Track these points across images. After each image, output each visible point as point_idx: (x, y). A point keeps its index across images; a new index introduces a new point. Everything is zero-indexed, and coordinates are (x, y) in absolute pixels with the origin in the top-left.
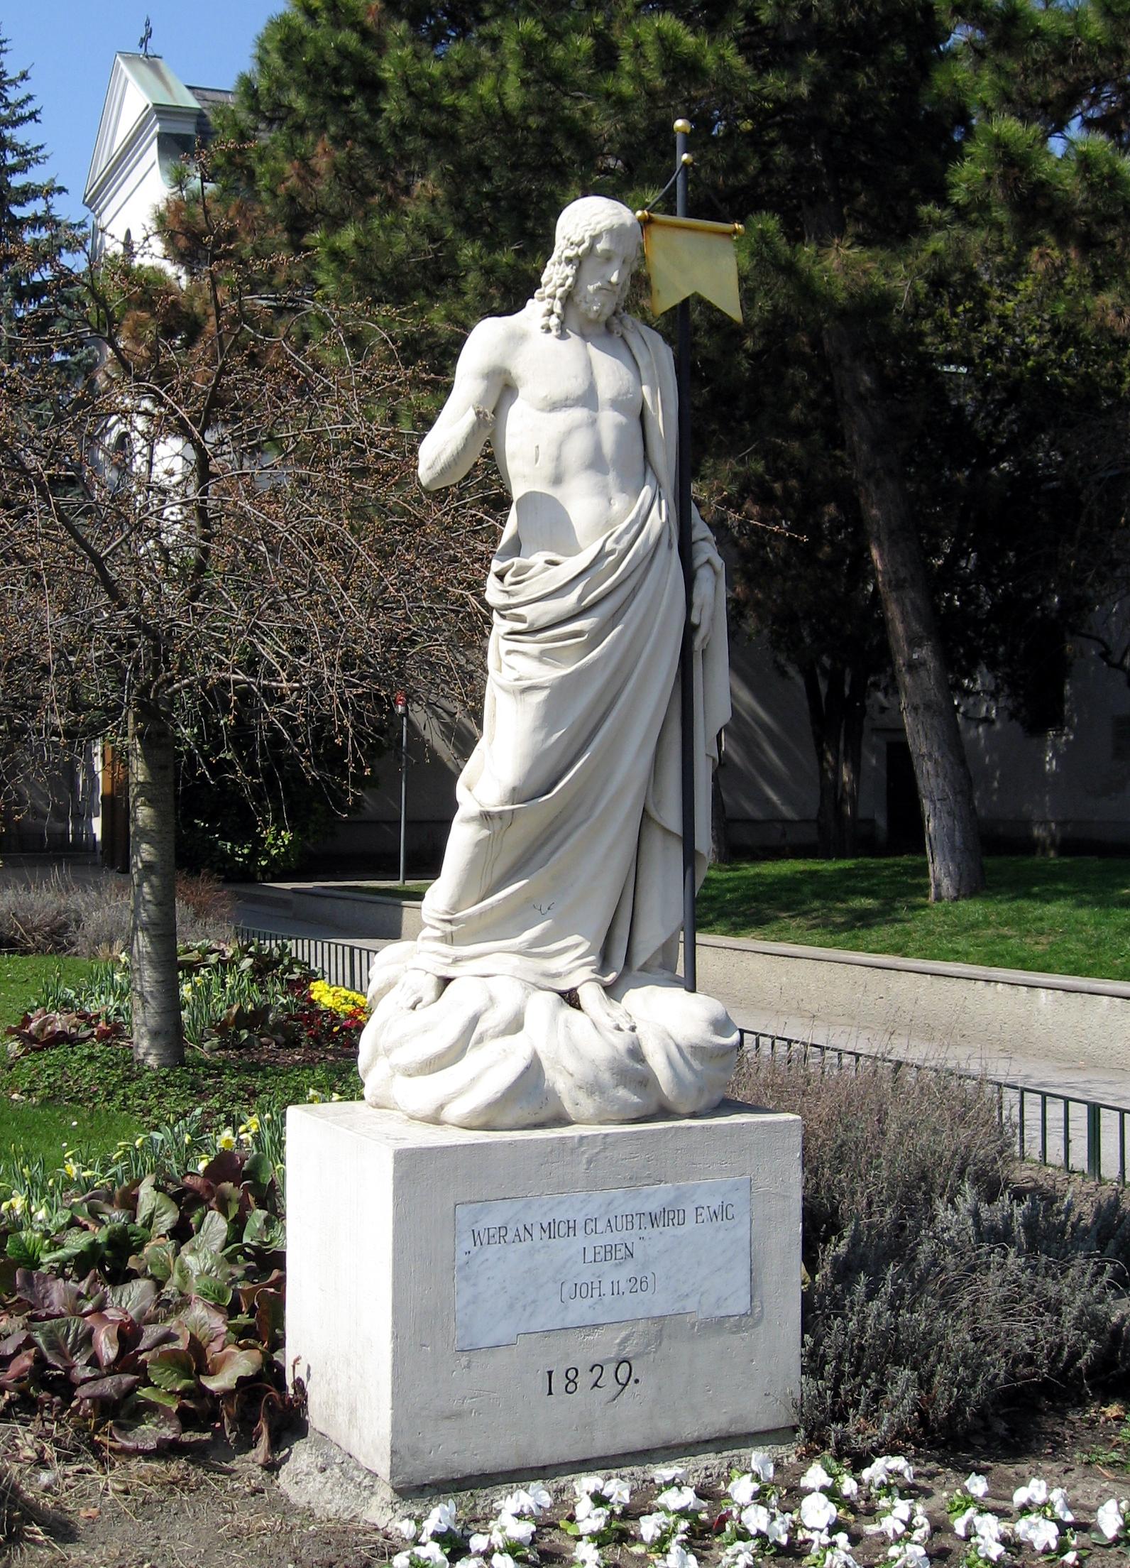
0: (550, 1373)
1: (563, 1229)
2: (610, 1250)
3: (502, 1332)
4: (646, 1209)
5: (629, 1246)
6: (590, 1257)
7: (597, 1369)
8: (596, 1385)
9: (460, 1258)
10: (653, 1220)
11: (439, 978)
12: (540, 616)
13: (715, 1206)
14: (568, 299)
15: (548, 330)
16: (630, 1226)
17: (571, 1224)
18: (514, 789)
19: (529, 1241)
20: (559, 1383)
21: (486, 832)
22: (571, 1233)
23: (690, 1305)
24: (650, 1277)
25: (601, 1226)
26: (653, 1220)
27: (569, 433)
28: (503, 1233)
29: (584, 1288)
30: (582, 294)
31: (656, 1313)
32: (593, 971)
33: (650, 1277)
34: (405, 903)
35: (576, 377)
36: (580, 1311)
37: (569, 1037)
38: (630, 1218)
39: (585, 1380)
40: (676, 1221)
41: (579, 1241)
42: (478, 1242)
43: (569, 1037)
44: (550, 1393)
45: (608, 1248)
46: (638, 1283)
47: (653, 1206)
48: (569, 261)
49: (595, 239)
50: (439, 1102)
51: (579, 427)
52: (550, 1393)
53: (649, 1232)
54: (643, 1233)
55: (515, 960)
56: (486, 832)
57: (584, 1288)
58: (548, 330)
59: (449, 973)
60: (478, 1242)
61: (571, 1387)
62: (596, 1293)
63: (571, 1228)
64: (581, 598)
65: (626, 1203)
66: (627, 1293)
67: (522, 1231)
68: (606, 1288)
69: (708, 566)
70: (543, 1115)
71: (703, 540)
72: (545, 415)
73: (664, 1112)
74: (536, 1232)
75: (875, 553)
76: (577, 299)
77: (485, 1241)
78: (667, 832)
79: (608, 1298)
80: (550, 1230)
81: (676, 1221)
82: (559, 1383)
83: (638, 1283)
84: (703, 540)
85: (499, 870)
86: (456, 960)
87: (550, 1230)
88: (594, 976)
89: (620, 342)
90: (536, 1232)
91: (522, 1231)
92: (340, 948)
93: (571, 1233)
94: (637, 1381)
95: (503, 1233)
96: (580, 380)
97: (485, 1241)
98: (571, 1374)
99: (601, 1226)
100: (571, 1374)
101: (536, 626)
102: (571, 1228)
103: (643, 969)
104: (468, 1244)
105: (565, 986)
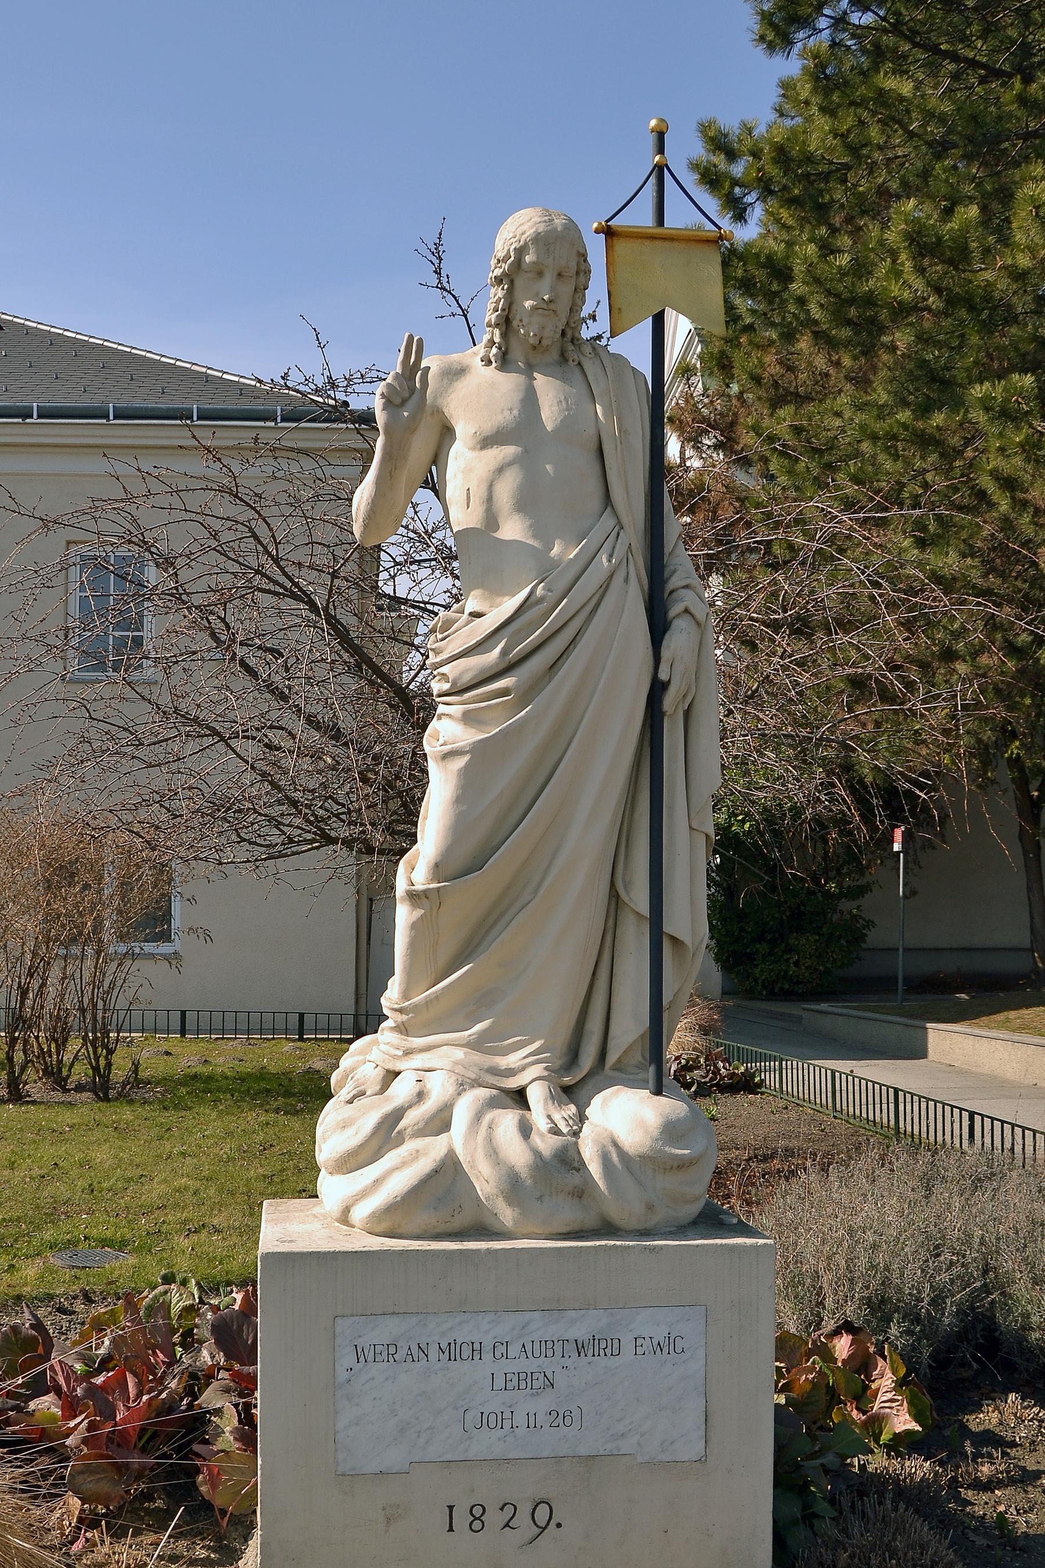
0: (451, 1508)
1: (467, 1352)
2: (524, 1379)
3: (394, 1458)
4: (572, 1334)
5: (549, 1375)
6: (500, 1383)
7: (509, 1510)
8: (507, 1525)
9: (342, 1375)
10: (580, 1348)
11: (388, 1071)
12: (461, 675)
13: (660, 1335)
14: (506, 322)
15: (489, 363)
16: (550, 1353)
17: (477, 1346)
18: (437, 865)
19: (423, 1362)
20: (461, 1519)
21: (419, 912)
22: (477, 1357)
23: (627, 1446)
24: (576, 1412)
25: (514, 1350)
26: (580, 1348)
27: (500, 470)
28: (392, 1350)
29: (493, 1417)
30: (518, 318)
31: (583, 1451)
32: (546, 1068)
33: (576, 1412)
34: (928, 1025)
35: (511, 410)
36: (486, 1443)
37: (490, 1140)
38: (550, 1345)
39: (495, 1518)
40: (608, 1351)
41: (486, 1365)
42: (362, 1359)
43: (490, 1140)
44: (451, 1529)
45: (523, 1376)
46: (559, 1418)
47: (580, 1332)
48: (499, 281)
49: (521, 251)
50: (344, 1204)
51: (510, 464)
52: (451, 1529)
53: (573, 1360)
54: (567, 1362)
55: (459, 1054)
56: (419, 912)
57: (493, 1417)
58: (489, 363)
59: (398, 1066)
60: (362, 1359)
61: (477, 1525)
62: (507, 1424)
63: (476, 1351)
64: (504, 653)
65: (541, 1327)
66: (546, 1427)
67: (415, 1350)
68: (520, 1419)
69: (687, 617)
70: (458, 1222)
71: (686, 587)
72: (477, 453)
73: (608, 1229)
74: (433, 1352)
75: (571, 556)
76: (515, 323)
77: (371, 1358)
78: (638, 914)
79: (522, 1431)
80: (451, 1352)
81: (608, 1351)
82: (461, 1519)
83: (559, 1418)
84: (686, 587)
85: (444, 955)
86: (408, 1053)
87: (451, 1352)
88: (546, 1073)
89: (577, 370)
90: (433, 1352)
91: (415, 1350)
92: (817, 1069)
93: (477, 1357)
94: (559, 1525)
95: (392, 1350)
96: (515, 412)
97: (371, 1358)
98: (477, 1511)
99: (514, 1350)
100: (477, 1511)
101: (460, 684)
102: (476, 1351)
103: (618, 1067)
104: (350, 1360)
105: (513, 1083)
